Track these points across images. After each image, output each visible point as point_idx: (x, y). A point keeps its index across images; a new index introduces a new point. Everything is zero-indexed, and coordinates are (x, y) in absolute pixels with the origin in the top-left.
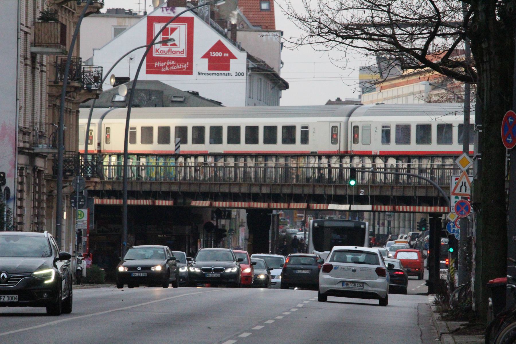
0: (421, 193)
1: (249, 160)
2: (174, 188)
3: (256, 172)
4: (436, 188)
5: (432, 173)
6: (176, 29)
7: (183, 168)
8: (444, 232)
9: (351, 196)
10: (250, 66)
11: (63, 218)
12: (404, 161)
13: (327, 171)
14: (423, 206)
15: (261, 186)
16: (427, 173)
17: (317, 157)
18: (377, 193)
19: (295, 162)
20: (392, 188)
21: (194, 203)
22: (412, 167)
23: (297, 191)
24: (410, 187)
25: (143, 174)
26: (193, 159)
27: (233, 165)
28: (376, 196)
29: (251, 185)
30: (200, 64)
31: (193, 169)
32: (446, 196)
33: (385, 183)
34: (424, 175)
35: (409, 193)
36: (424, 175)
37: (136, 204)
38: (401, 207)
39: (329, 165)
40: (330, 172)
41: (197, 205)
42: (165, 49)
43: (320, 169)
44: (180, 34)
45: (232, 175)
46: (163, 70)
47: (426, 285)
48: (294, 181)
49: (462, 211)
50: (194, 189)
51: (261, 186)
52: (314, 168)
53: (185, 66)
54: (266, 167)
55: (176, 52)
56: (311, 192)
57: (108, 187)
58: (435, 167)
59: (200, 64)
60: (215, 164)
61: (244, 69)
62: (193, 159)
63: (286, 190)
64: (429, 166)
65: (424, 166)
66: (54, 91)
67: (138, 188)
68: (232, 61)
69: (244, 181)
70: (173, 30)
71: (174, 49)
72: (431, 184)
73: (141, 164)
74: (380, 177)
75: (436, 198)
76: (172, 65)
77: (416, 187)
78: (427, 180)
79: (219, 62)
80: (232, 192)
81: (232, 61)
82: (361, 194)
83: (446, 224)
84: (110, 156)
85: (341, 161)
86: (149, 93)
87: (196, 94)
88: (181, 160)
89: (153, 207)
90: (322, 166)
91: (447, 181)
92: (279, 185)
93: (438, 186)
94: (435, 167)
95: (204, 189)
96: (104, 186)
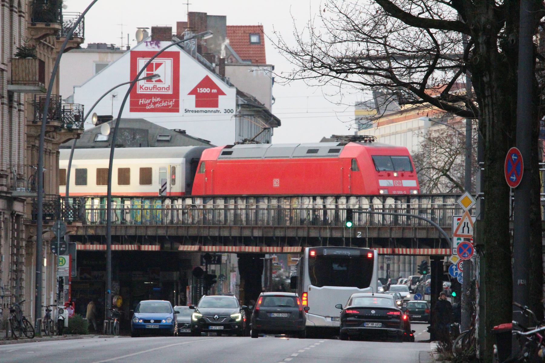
0: (422, 235)
1: (240, 201)
2: (161, 232)
3: (247, 214)
4: (437, 229)
5: (433, 213)
6: (160, 64)
7: (170, 211)
8: (447, 275)
9: (347, 239)
10: (240, 102)
11: (43, 265)
12: (403, 200)
13: (322, 212)
14: (424, 248)
15: (253, 228)
16: (427, 213)
17: (311, 198)
18: (375, 235)
19: (288, 203)
20: (391, 229)
21: (182, 248)
22: (411, 207)
23: (291, 234)
24: (410, 229)
25: (128, 217)
26: (180, 201)
27: (223, 207)
28: (375, 239)
29: (242, 228)
30: (187, 101)
31: (180, 212)
32: (448, 238)
33: (383, 224)
34: (424, 216)
35: (409, 235)
36: (424, 216)
37: (120, 249)
38: (400, 249)
39: (324, 206)
40: (325, 213)
41: (185, 249)
42: (150, 85)
43: (314, 210)
44: (165, 69)
45: (222, 217)
46: (147, 108)
47: (428, 331)
48: (288, 224)
49: (465, 253)
50: (182, 232)
51: (253, 228)
52: (308, 209)
53: (171, 103)
54: (257, 209)
55: (161, 89)
56: (305, 235)
57: (91, 232)
58: (436, 207)
59: (187, 101)
60: (204, 206)
61: (233, 106)
62: (180, 201)
63: (279, 233)
64: (429, 206)
65: (424, 206)
66: (33, 132)
67: (122, 232)
68: (220, 97)
69: (235, 224)
70: (158, 65)
71: (159, 85)
72: (432, 225)
73: (126, 207)
74: (378, 218)
75: (437, 240)
76: (157, 103)
77: (416, 229)
78: (427, 221)
79: (207, 98)
80: (222, 235)
81: (220, 97)
82: (358, 237)
83: (448, 267)
84: (93, 199)
85: (336, 202)
86: (133, 131)
87: (183, 133)
88: (168, 202)
89: (139, 253)
90: (316, 207)
91: (448, 222)
92: (271, 227)
93: (440, 228)
94: (436, 207)
95: (193, 232)
96: (86, 231)
